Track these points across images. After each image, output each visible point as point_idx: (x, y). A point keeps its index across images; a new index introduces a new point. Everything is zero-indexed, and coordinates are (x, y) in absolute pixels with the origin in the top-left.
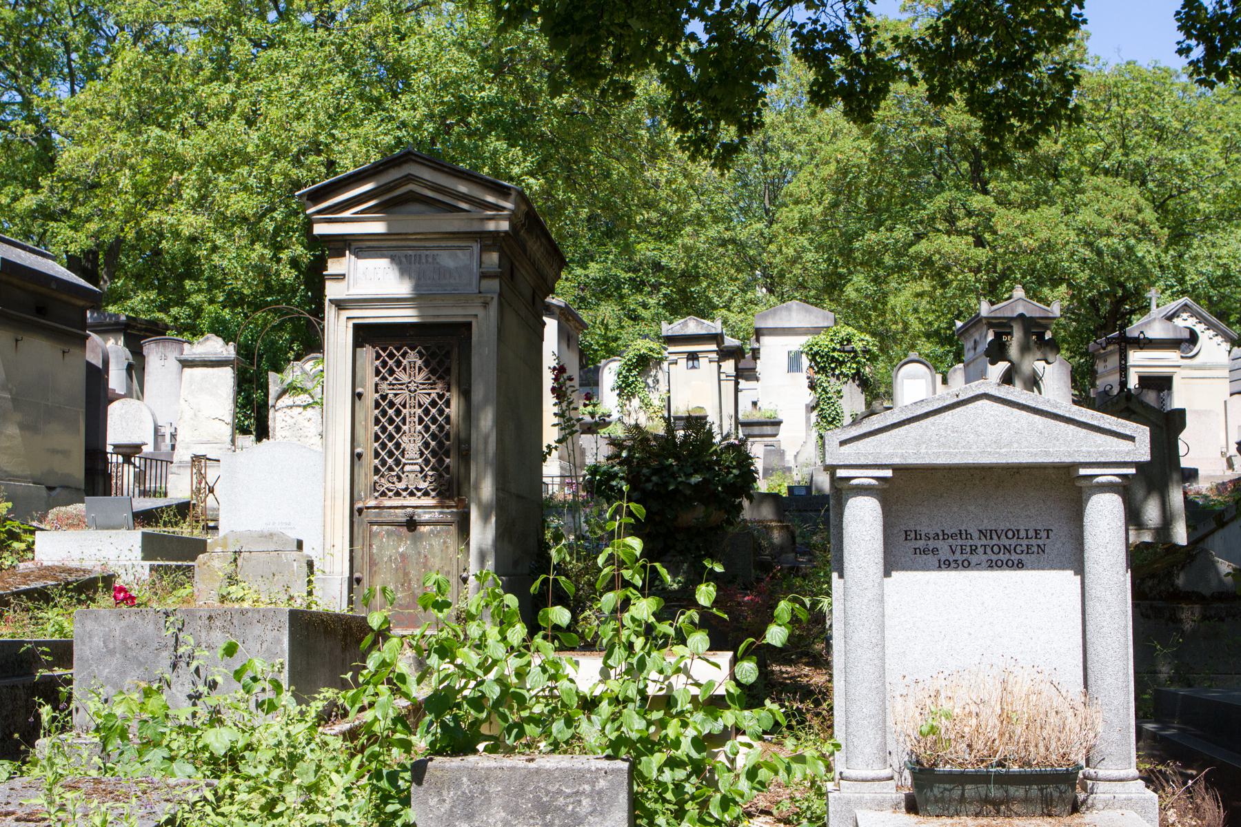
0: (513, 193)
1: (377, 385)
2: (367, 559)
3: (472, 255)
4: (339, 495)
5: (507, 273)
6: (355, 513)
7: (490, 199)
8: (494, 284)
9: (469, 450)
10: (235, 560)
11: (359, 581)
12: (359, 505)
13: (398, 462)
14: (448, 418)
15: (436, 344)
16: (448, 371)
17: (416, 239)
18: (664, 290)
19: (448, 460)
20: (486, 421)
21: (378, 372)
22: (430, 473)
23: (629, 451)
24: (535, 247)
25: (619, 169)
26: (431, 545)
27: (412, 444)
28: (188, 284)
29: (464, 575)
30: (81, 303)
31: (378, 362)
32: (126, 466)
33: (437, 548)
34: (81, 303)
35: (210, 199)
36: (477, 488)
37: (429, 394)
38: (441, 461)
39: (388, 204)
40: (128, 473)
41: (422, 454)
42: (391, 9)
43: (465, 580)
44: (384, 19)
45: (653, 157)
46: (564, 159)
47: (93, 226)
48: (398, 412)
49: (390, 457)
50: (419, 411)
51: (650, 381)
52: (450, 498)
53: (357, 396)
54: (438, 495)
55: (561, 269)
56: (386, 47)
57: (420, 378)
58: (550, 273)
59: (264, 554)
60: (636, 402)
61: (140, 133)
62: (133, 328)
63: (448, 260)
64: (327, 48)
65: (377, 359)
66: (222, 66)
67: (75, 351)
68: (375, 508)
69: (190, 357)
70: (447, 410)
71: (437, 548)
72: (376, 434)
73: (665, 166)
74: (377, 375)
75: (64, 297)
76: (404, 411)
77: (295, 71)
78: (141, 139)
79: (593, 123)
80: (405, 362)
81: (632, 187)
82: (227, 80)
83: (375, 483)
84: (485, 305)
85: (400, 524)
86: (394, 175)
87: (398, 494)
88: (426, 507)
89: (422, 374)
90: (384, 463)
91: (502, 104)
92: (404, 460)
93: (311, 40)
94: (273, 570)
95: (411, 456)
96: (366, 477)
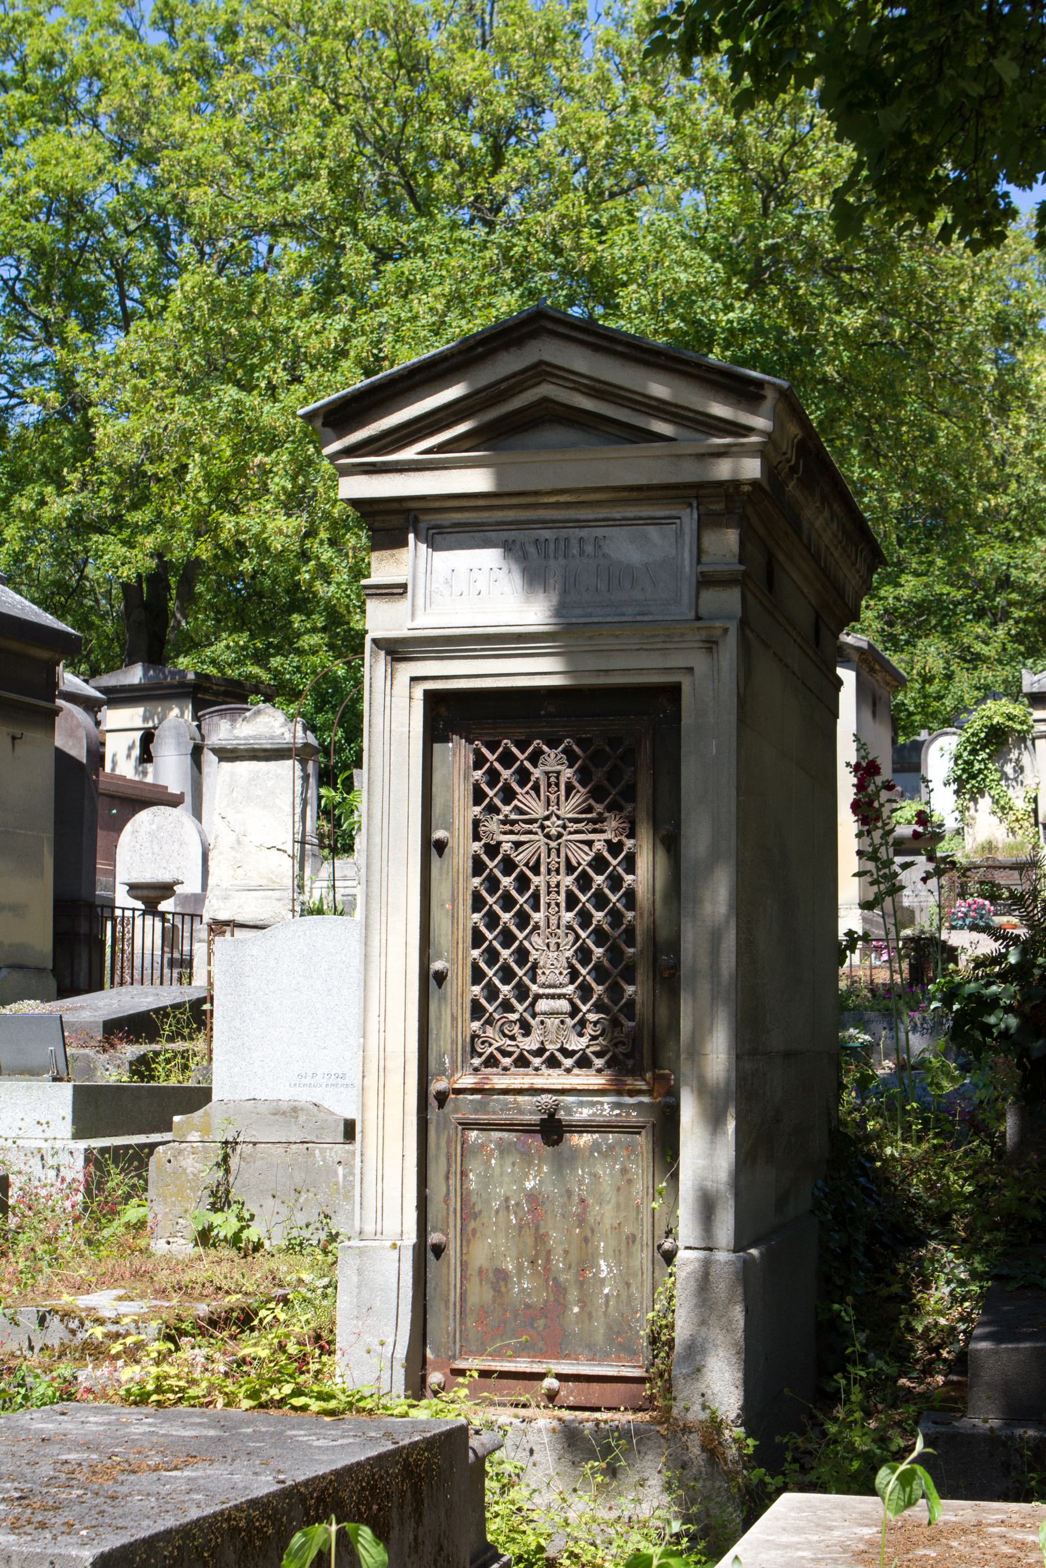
0: (770, 395)
1: (476, 823)
2: (456, 1203)
3: (679, 535)
4: (395, 1064)
5: (759, 577)
6: (429, 1102)
7: (720, 410)
8: (730, 599)
9: (676, 967)
10: (226, 1158)
11: (439, 1250)
12: (438, 1085)
13: (522, 992)
14: (630, 896)
15: (603, 733)
16: (630, 794)
17: (557, 505)
18: (1017, 613)
19: (630, 989)
20: (717, 898)
21: (479, 796)
22: (592, 1017)
23: (1024, 953)
24: (818, 520)
25: (945, 430)
26: (595, 1176)
27: (552, 954)
28: (296, 618)
29: (667, 1245)
30: (45, 655)
31: (478, 774)
32: (149, 919)
33: (607, 1184)
34: (45, 655)
35: (310, 490)
36: (696, 1052)
37: (590, 843)
38: (615, 991)
39: (497, 428)
40: (147, 935)
41: (574, 975)
42: (586, 189)
43: (669, 1257)
44: (573, 204)
45: (1002, 409)
46: (860, 416)
47: (149, 542)
48: (523, 883)
49: (505, 981)
50: (568, 881)
51: (1009, 769)
52: (637, 1072)
53: (433, 848)
54: (609, 1065)
55: (872, 570)
56: (577, 247)
57: (568, 809)
58: (851, 578)
59: (280, 1149)
60: (985, 803)
61: (209, 396)
62: (206, 690)
63: (627, 548)
64: (487, 254)
65: (477, 766)
66: (330, 289)
67: (33, 735)
68: (473, 1091)
69: (229, 744)
70: (628, 879)
71: (607, 1184)
72: (476, 931)
73: (1023, 421)
74: (477, 802)
75: (15, 646)
76: (536, 880)
77: (438, 290)
78: (209, 405)
79: (907, 356)
80: (537, 773)
81: (971, 458)
82: (337, 310)
83: (474, 1036)
84: (711, 645)
85: (526, 1129)
86: (508, 364)
87: (522, 1062)
88: (583, 1090)
89: (575, 800)
90: (492, 993)
91: (761, 331)
92: (534, 988)
93: (462, 241)
94: (298, 1178)
95: (552, 979)
96: (453, 1024)
